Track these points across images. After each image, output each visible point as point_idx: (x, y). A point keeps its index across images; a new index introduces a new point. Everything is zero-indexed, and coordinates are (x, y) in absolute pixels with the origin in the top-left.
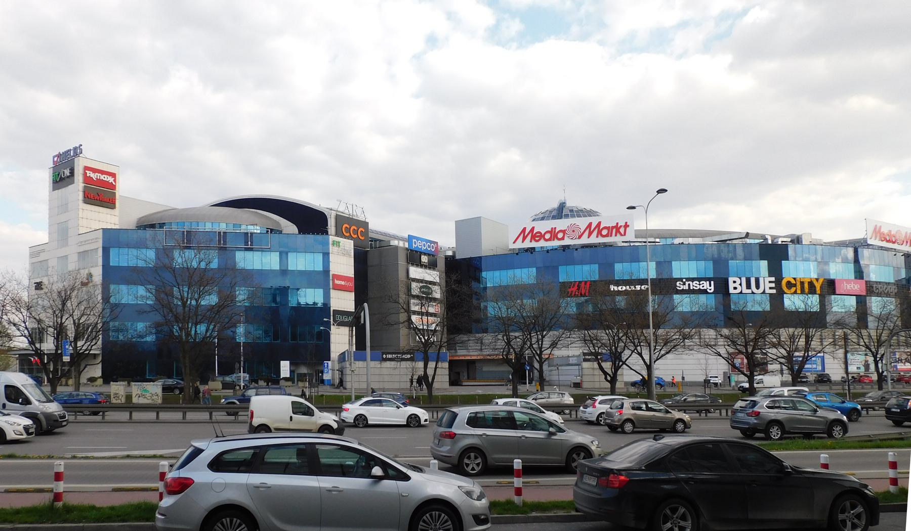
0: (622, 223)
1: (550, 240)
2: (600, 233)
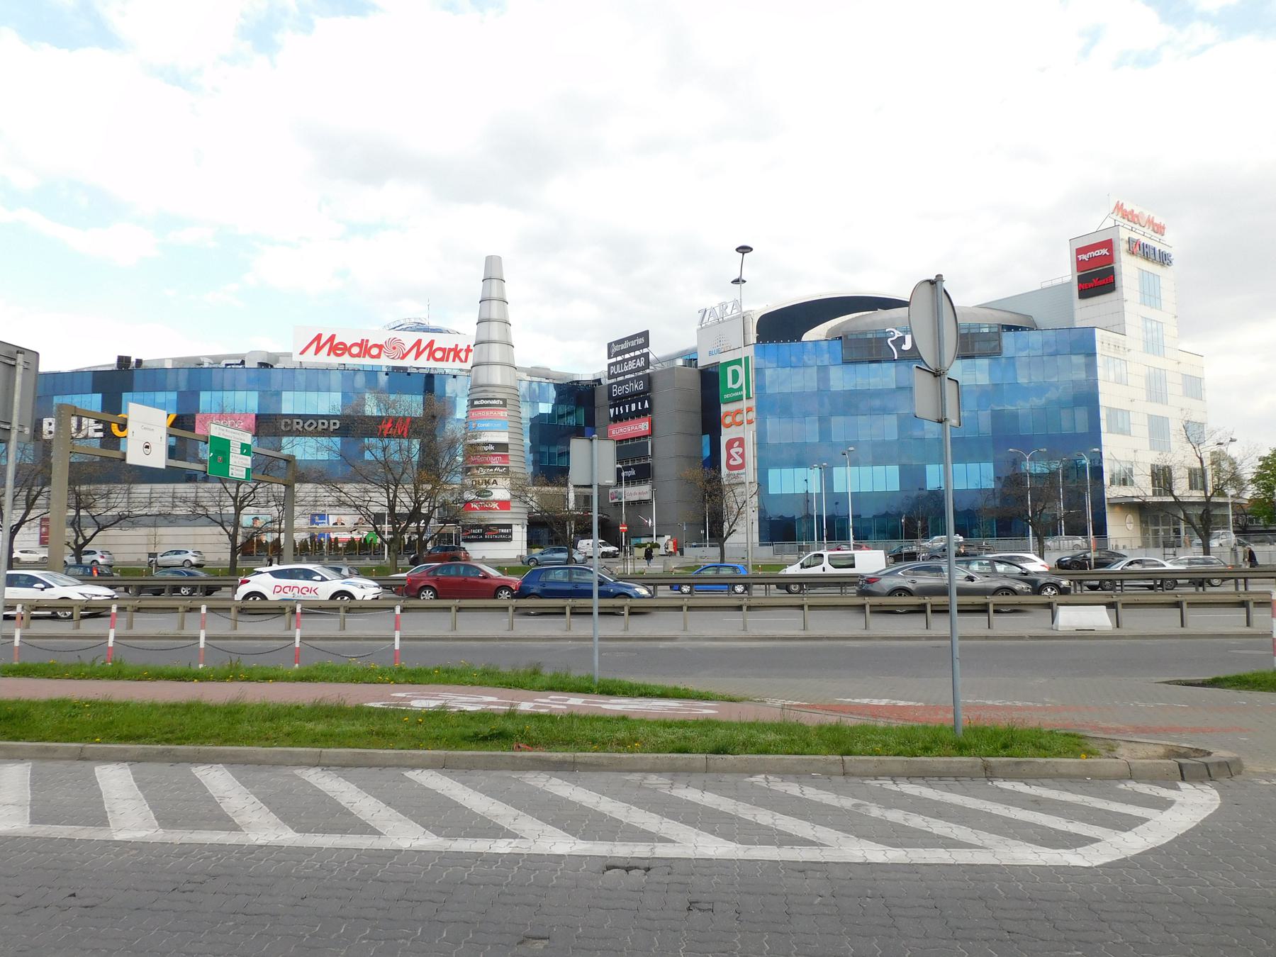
0: (463, 346)
1: (358, 355)
2: (431, 355)
